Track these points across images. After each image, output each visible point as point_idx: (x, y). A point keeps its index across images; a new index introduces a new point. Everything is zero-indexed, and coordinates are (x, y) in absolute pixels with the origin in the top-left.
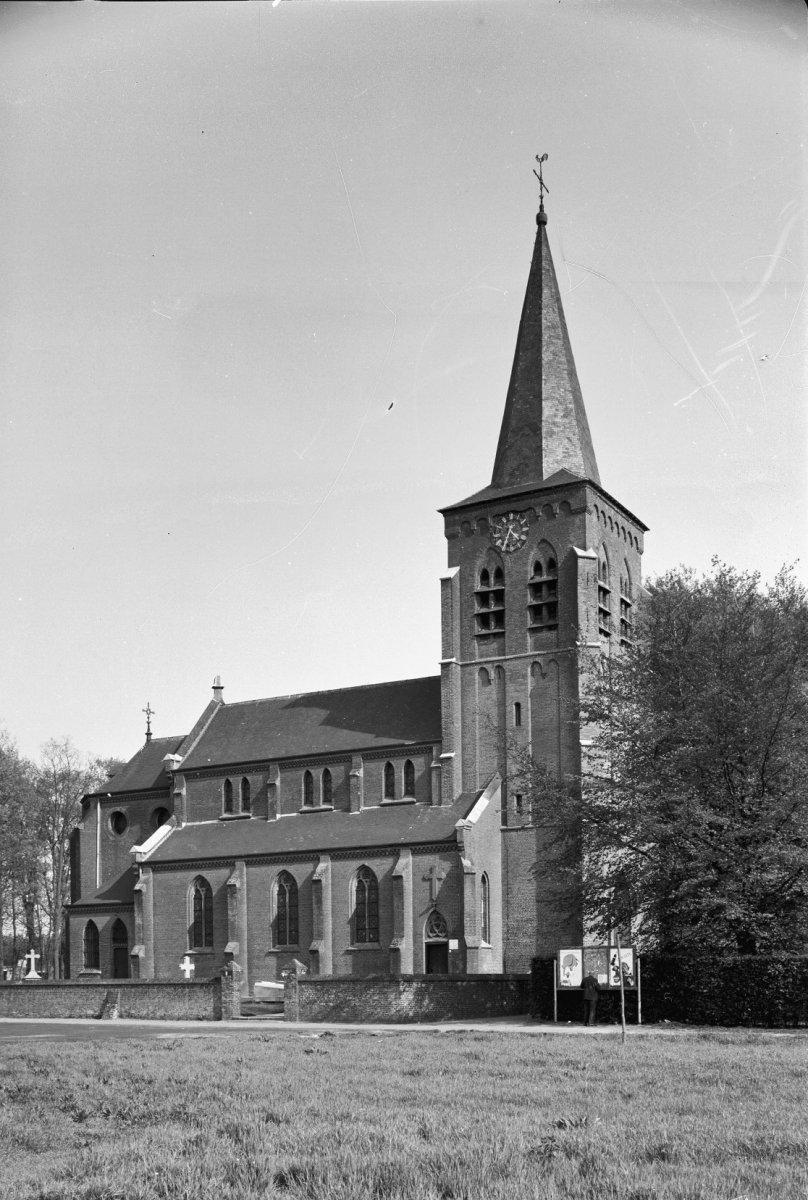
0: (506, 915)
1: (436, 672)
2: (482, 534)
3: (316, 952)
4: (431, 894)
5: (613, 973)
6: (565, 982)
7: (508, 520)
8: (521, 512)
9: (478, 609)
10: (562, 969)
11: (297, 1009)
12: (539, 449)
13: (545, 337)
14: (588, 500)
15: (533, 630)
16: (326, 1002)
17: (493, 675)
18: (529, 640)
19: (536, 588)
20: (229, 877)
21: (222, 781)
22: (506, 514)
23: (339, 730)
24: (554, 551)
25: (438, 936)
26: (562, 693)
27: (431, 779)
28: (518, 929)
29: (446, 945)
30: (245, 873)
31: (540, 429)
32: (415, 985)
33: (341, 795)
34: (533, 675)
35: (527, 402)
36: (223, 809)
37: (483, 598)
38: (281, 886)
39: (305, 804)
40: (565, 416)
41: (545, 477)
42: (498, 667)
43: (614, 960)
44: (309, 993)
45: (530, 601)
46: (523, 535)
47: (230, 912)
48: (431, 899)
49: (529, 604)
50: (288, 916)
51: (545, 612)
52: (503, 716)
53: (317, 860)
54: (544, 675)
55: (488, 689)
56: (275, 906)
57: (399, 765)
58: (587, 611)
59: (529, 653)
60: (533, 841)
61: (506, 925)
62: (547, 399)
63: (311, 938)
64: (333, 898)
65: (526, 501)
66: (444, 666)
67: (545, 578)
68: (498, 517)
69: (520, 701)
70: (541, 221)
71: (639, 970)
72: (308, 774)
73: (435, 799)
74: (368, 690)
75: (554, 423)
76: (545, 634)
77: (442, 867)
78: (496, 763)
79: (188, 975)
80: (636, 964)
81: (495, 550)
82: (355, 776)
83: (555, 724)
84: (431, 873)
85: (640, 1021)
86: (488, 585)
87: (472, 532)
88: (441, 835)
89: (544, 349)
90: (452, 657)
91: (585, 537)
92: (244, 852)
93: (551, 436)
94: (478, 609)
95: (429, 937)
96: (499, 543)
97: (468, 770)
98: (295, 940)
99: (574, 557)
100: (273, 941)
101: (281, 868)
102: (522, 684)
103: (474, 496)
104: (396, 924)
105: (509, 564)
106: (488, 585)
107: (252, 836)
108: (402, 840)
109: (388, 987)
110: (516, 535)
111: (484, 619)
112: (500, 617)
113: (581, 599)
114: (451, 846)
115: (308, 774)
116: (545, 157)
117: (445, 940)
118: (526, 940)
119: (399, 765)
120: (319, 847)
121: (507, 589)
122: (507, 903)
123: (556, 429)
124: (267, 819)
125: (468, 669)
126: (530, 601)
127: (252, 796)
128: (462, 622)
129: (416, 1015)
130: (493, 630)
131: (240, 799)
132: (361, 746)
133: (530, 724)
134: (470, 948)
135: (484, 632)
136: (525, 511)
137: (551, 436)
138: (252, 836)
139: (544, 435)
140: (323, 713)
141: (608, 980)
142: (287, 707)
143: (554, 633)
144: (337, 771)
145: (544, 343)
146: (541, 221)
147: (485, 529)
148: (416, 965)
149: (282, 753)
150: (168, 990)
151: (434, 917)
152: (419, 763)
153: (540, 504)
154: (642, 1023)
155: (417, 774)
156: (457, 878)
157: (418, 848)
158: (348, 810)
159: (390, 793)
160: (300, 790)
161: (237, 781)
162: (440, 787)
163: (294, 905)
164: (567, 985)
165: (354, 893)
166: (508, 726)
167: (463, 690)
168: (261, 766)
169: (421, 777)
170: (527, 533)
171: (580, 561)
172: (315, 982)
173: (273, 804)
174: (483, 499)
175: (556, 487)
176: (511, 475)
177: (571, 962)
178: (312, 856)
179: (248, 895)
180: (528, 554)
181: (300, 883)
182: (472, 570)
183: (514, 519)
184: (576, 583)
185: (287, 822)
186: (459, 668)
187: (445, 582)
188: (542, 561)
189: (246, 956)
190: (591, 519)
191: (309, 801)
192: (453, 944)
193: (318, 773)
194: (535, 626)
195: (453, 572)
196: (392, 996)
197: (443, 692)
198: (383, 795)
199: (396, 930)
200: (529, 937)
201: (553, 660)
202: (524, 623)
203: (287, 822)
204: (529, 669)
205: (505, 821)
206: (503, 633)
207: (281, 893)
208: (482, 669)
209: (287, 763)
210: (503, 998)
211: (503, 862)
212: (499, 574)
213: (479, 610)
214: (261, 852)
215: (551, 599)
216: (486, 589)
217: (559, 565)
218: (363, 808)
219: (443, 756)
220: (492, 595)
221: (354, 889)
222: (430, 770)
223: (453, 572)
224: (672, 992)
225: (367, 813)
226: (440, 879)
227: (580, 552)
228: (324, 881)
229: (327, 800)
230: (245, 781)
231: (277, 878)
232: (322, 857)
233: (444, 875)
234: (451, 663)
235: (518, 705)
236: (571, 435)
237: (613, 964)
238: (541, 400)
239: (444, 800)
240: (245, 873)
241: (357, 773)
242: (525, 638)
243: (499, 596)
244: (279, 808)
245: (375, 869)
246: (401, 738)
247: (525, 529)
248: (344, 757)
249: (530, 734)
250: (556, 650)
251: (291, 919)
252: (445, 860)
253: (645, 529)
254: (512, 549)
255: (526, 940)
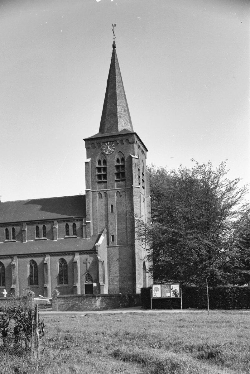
0: (109, 275)
1: (84, 193)
2: (98, 148)
3: (46, 288)
4: (87, 268)
5: (172, 293)
6: (155, 296)
7: (108, 144)
8: (112, 142)
9: (97, 173)
10: (153, 292)
11: (57, 307)
12: (117, 122)
13: (117, 85)
14: (135, 139)
15: (117, 181)
16: (68, 304)
17: (103, 195)
18: (116, 184)
19: (117, 167)
20: (11, 262)
21: (5, 229)
22: (107, 142)
23: (47, 212)
24: (124, 156)
25: (89, 282)
26: (127, 202)
27: (82, 230)
28: (113, 279)
29: (92, 285)
30: (17, 260)
31: (117, 115)
32: (100, 298)
33: (50, 235)
34: (117, 196)
35: (112, 106)
36: (5, 238)
37: (99, 169)
38: (31, 265)
39: (66, 235)
40: (124, 112)
41: (119, 131)
42: (105, 193)
43: (172, 288)
44: (62, 301)
45: (115, 171)
46: (113, 150)
47: (12, 274)
48: (87, 270)
49: (115, 172)
50: (34, 275)
51: (121, 175)
52: (107, 209)
53: (45, 256)
54: (121, 196)
55: (101, 200)
56: (29, 272)
57: (71, 225)
58: (136, 176)
59: (116, 188)
60: (118, 251)
61: (109, 278)
62: (119, 106)
63: (44, 283)
64: (51, 269)
65: (114, 138)
66: (87, 192)
67: (120, 164)
68: (104, 143)
69: (113, 204)
70: (114, 47)
71: (181, 292)
72: (37, 227)
73: (84, 236)
74: (55, 199)
75: (121, 114)
76: (121, 183)
77: (90, 259)
78: (104, 225)
79: (5, 296)
80: (180, 290)
81: (104, 154)
82: (55, 228)
83: (125, 212)
84: (86, 261)
85: (182, 308)
86: (101, 165)
87: (95, 147)
88: (90, 248)
89: (117, 89)
90: (89, 189)
91: (134, 151)
92: (17, 253)
93: (120, 118)
94: (97, 173)
95: (86, 282)
96: (104, 151)
97: (95, 227)
98: (37, 283)
99: (131, 158)
100: (29, 284)
101: (31, 259)
102: (113, 199)
103: (95, 135)
104: (75, 278)
105: (108, 159)
106: (101, 165)
107: (46, 245)
108: (75, 250)
109: (92, 298)
110: (110, 149)
111: (99, 177)
112: (105, 176)
113: (134, 171)
114: (93, 251)
115: (37, 227)
116: (114, 26)
117: (92, 283)
118: (116, 283)
119: (71, 225)
120: (45, 252)
121: (107, 167)
122: (109, 271)
123: (122, 116)
124: (22, 242)
125: (94, 193)
126: (115, 171)
127: (16, 234)
128: (92, 177)
129: (101, 308)
130: (103, 180)
131: (12, 235)
132: (56, 218)
133: (116, 212)
134: (102, 286)
135: (100, 181)
136: (113, 142)
137: (120, 118)
138: (46, 245)
139: (118, 117)
140: (39, 207)
141: (170, 295)
142: (26, 204)
143: (124, 182)
144: (48, 226)
145: (117, 87)
146: (114, 47)
147: (100, 146)
148: (81, 292)
149: (27, 220)
150: (5, 301)
151: (87, 276)
152: (78, 224)
153: (119, 140)
154: (183, 309)
155: (77, 228)
156: (96, 262)
157: (82, 252)
158: (53, 239)
159: (68, 234)
160: (34, 232)
161: (10, 229)
162: (86, 233)
163: (36, 272)
164: (155, 297)
165: (58, 267)
166: (109, 212)
167: (93, 200)
168: (20, 224)
169: (79, 229)
170: (114, 149)
171: (133, 159)
172: (64, 297)
173: (24, 238)
174: (95, 137)
175: (124, 134)
176: (107, 129)
177: (157, 289)
178: (43, 255)
179: (19, 268)
180: (115, 156)
181: (38, 264)
182: (95, 160)
183: (110, 144)
184: (132, 166)
185: (30, 243)
186: (91, 192)
187: (86, 163)
188: (119, 158)
189: (18, 289)
190: (135, 145)
191: (38, 235)
192: (95, 285)
193: (41, 227)
194: (117, 180)
195: (89, 160)
196: (94, 302)
197: (87, 200)
198: (65, 235)
199: (74, 279)
200: (117, 282)
201: (124, 191)
202: (113, 178)
203: (30, 243)
204: (116, 194)
205: (108, 244)
206: (107, 181)
207: (31, 267)
208: (99, 193)
209: (29, 223)
210: (125, 302)
211: (108, 258)
212: (105, 162)
213: (98, 173)
214: (23, 253)
215: (123, 171)
216: (100, 166)
217: (126, 160)
218: (58, 239)
219: (87, 222)
220: (102, 169)
221: (58, 266)
222: (82, 226)
223: (89, 160)
224: (190, 300)
225: (60, 241)
226: (89, 263)
227: (133, 156)
228: (48, 264)
229: (44, 236)
230: (13, 229)
231: (29, 262)
232: (47, 255)
233: (91, 262)
234: (89, 190)
235: (112, 206)
236: (126, 118)
237: (172, 290)
238: (117, 106)
239: (87, 237)
240: (17, 260)
241: (56, 227)
242: (114, 183)
243: (105, 169)
244: (27, 239)
245: (66, 259)
246: (71, 215)
247: (113, 147)
248: (51, 221)
249: (116, 215)
250: (125, 188)
251: (35, 276)
252: (91, 256)
253: (147, 151)
254: (109, 154)
255: (116, 283)
